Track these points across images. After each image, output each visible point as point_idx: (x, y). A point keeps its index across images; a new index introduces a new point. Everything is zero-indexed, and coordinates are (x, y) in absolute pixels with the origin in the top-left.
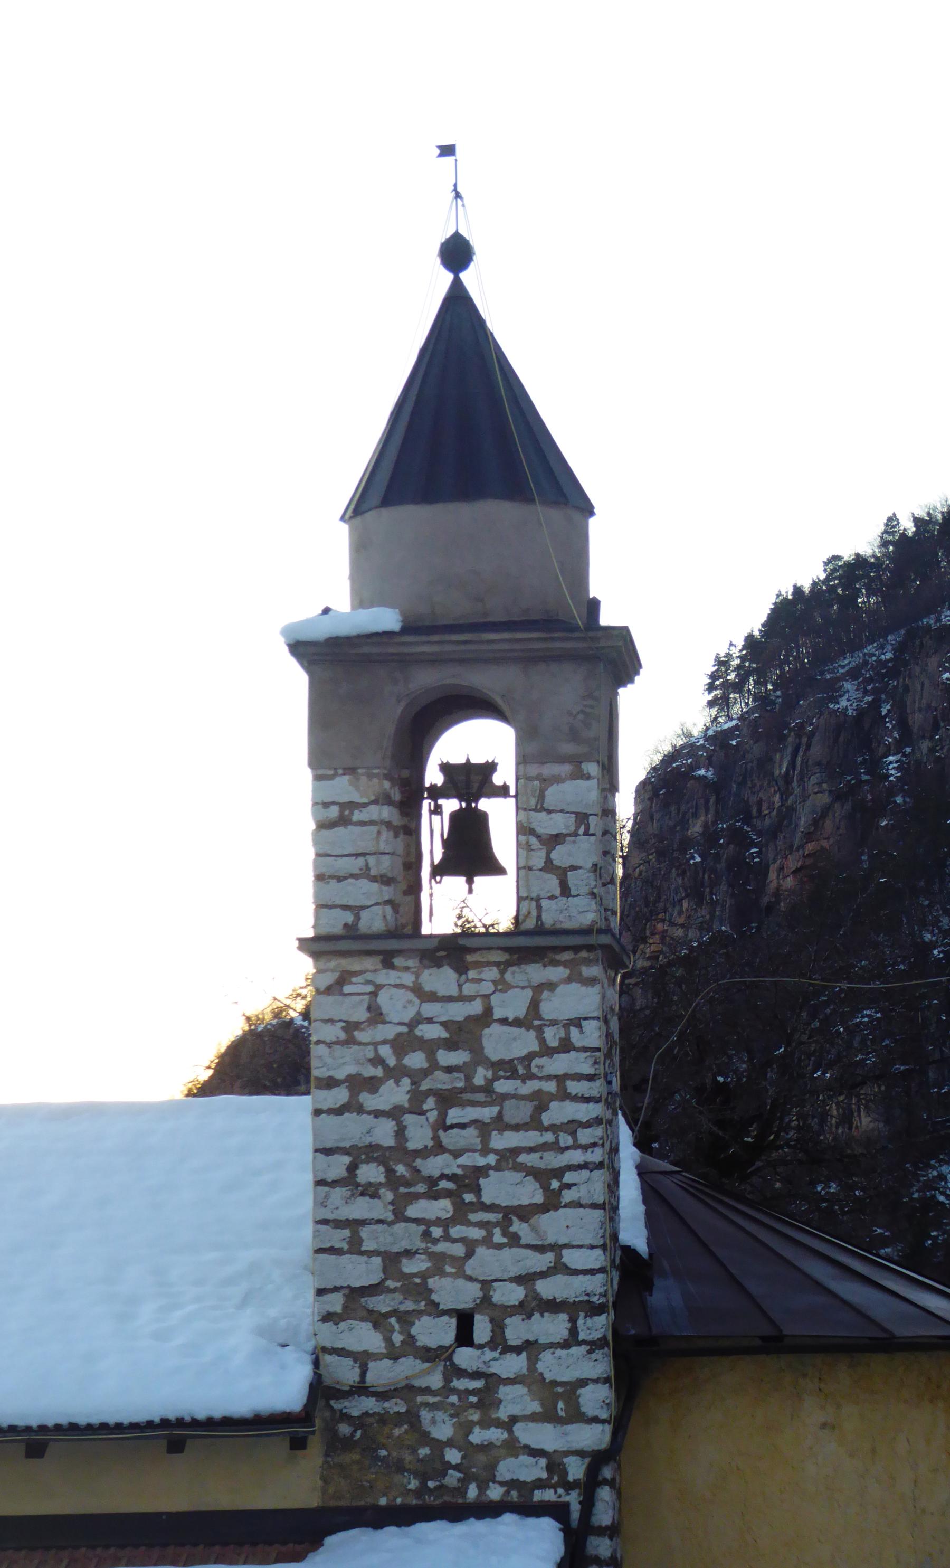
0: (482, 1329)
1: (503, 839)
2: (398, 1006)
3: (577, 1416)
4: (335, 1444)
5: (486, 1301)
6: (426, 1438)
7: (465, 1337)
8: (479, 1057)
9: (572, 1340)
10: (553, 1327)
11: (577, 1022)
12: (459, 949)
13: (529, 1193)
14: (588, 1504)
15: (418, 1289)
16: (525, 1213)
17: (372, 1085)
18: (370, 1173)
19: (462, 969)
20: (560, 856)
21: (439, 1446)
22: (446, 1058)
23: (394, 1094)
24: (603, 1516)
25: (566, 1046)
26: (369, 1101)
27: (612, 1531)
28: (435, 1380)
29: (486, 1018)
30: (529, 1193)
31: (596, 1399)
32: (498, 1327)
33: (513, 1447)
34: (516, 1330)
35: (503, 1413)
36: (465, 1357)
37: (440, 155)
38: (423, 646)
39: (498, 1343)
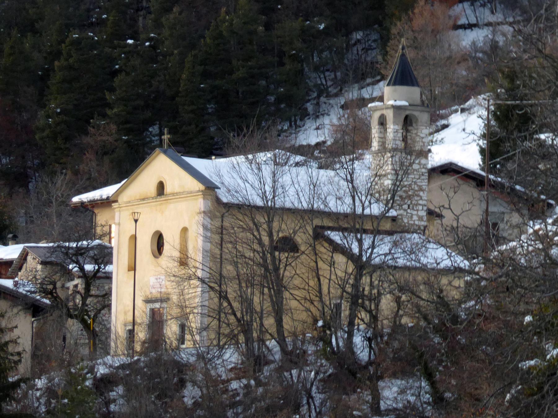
3: (422, 220)
6: (403, 222)
10: (421, 208)
28: (405, 214)
32: (413, 207)
35: (413, 219)
36: (409, 211)
38: (410, 108)
39: (413, 209)
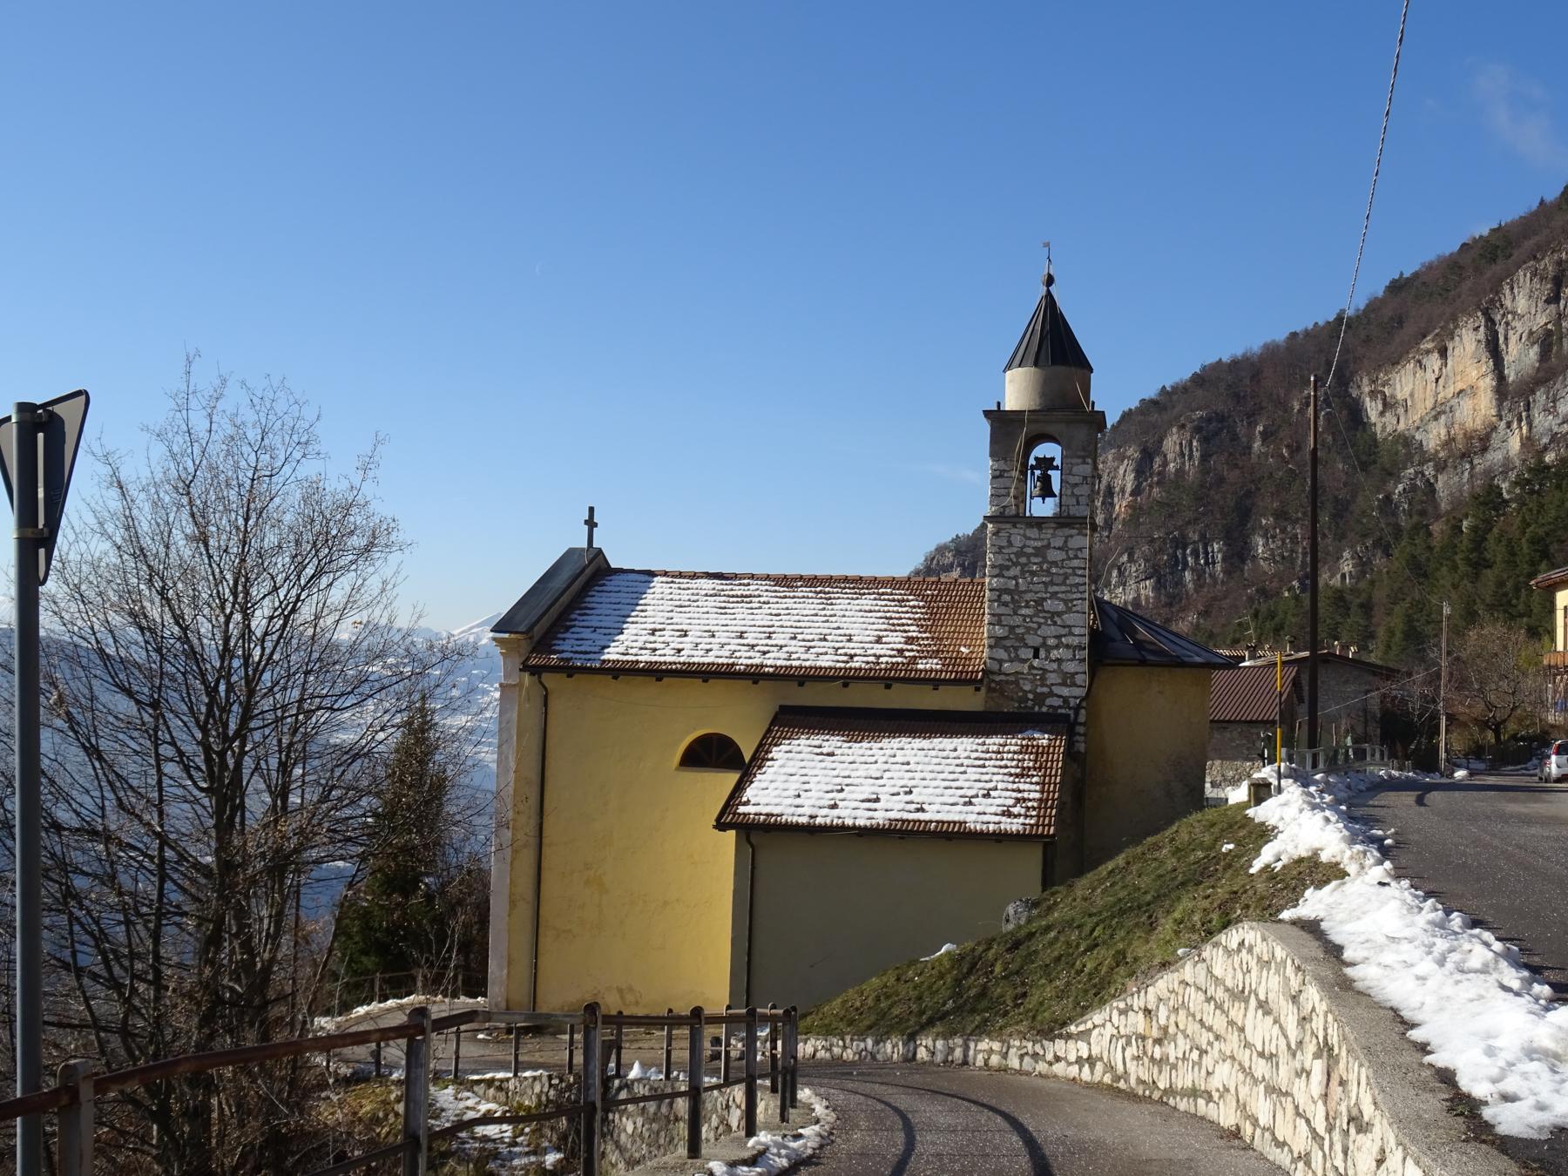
0: (1042, 654)
1: (1056, 488)
2: (1017, 541)
3: (1074, 685)
4: (990, 690)
5: (1044, 644)
7: (1036, 656)
8: (1045, 560)
9: (1073, 659)
11: (1080, 549)
12: (1039, 523)
13: (1061, 607)
14: (1077, 714)
15: (1021, 639)
16: (1059, 614)
17: (1008, 568)
18: (1006, 598)
19: (1040, 529)
20: (1077, 491)
21: (1026, 692)
22: (1034, 560)
23: (1015, 571)
24: (1082, 719)
25: (1076, 557)
26: (1006, 573)
27: (1084, 724)
29: (1048, 546)
30: (1061, 607)
31: (1082, 679)
33: (1051, 694)
34: (1055, 654)
36: (1036, 663)
37: (987, 414)
